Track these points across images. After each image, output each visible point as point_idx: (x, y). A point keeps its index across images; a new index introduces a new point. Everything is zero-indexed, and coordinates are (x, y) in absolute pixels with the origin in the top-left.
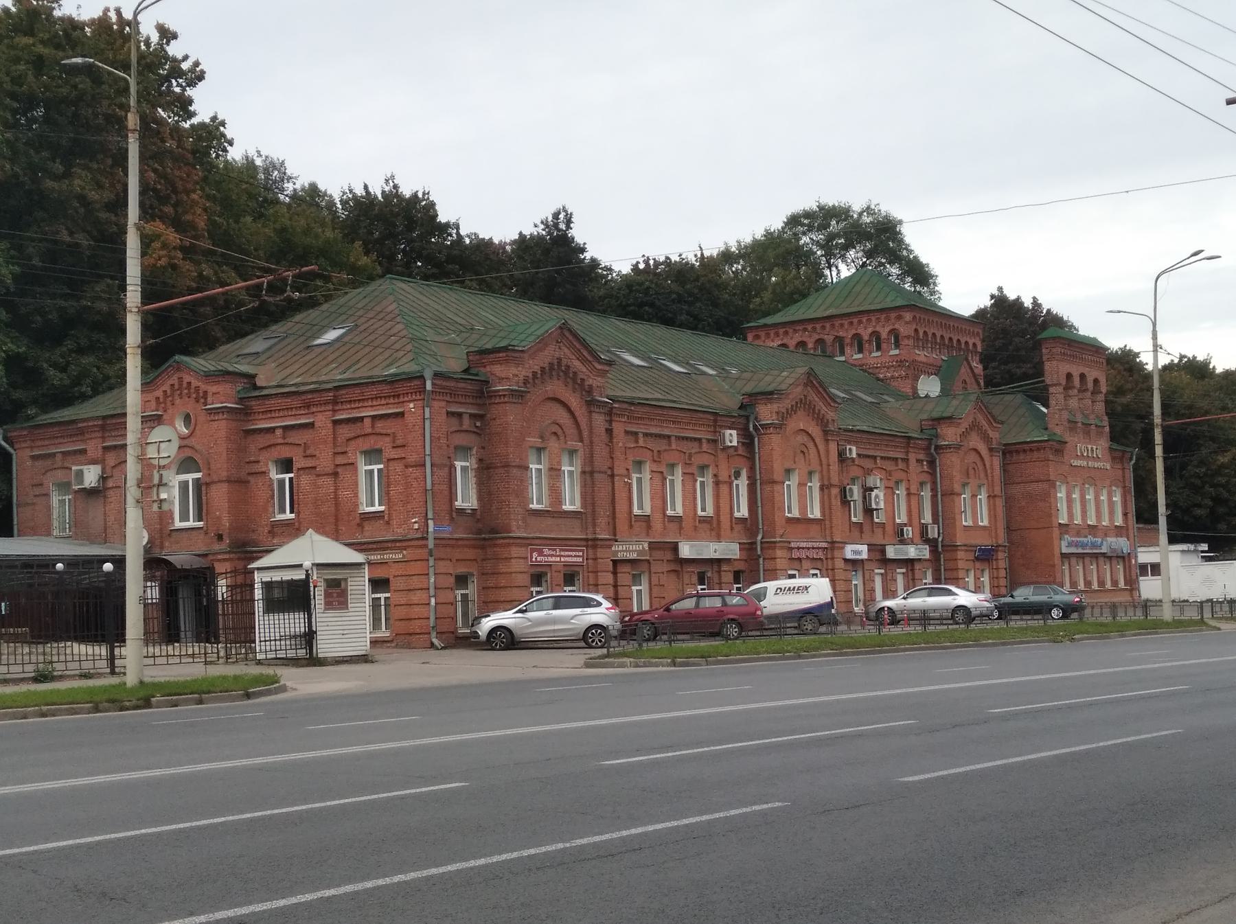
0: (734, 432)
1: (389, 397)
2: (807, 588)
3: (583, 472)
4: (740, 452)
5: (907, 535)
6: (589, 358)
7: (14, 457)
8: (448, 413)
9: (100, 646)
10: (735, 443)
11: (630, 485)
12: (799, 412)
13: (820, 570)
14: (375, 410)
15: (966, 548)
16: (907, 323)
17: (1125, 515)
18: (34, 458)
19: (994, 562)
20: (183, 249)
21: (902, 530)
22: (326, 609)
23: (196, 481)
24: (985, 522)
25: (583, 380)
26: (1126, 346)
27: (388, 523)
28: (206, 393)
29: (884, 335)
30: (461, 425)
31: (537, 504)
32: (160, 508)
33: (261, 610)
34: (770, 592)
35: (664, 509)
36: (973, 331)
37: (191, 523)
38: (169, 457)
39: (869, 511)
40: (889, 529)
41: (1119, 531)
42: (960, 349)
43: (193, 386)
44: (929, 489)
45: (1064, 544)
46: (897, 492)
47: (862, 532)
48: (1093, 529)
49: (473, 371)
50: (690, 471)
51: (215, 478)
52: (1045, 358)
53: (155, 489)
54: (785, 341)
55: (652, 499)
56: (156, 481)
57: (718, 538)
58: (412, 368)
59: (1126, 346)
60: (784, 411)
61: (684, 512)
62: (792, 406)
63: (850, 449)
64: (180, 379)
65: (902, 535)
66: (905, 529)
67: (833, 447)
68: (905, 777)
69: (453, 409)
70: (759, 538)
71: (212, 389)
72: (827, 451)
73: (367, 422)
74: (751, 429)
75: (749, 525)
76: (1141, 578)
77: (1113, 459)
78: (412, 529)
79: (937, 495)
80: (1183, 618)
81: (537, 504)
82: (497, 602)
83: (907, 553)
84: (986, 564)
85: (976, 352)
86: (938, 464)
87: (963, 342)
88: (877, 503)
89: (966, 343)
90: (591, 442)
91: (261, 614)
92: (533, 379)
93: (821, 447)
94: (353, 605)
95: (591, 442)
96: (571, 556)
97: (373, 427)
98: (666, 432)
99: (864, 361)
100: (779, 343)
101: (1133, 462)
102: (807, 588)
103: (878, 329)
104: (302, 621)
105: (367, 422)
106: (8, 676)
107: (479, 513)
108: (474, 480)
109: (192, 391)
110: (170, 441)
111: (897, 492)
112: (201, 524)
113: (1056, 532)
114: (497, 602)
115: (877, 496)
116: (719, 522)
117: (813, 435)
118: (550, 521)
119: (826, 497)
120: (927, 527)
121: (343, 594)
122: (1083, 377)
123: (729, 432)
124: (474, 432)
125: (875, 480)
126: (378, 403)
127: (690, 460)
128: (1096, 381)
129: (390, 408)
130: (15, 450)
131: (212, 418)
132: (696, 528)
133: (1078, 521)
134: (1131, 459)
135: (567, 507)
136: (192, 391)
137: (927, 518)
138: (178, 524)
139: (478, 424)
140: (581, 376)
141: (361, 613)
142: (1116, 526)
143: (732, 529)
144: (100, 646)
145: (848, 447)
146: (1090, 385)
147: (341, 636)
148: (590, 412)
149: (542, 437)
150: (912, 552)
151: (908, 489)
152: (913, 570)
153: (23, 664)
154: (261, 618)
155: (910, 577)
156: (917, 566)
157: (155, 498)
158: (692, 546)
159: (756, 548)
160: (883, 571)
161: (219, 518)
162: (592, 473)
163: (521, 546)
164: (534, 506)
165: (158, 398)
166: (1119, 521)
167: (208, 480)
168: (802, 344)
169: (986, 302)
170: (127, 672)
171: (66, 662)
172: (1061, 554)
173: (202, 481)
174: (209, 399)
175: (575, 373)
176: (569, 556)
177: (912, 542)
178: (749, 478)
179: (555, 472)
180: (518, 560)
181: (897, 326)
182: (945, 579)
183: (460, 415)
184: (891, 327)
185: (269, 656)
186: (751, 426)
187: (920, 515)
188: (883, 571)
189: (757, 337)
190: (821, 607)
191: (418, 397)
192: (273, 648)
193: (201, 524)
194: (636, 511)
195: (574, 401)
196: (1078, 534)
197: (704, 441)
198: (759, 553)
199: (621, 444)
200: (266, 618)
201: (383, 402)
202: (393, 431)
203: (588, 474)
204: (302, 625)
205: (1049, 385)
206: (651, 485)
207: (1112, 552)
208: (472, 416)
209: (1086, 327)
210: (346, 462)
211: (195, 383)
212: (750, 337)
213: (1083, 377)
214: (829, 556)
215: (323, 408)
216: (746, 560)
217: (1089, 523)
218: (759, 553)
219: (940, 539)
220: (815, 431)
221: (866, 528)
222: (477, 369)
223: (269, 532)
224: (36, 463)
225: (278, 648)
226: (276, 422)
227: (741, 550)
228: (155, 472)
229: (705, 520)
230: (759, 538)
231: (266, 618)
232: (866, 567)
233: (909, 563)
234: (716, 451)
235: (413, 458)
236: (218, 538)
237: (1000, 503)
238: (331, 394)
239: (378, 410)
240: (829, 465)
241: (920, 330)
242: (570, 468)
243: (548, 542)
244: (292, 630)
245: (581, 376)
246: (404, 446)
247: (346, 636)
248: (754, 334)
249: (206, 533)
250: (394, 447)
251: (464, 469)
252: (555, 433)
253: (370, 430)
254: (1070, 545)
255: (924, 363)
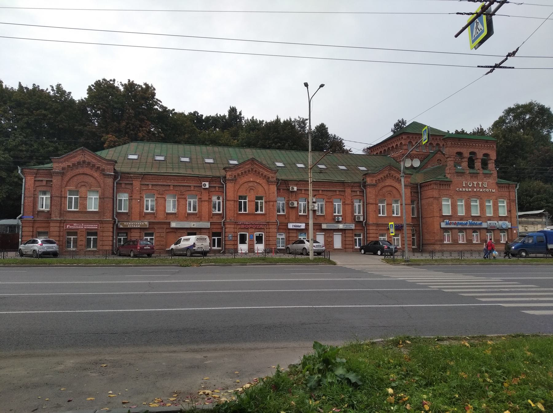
8: (351, 191)
15: (376, 225)
16: (405, 139)
26: (253, 117)
31: (74, 209)
59: (253, 117)
68: (524, 310)
80: (443, 257)
81: (74, 209)
84: (400, 232)
96: (91, 226)
98: (169, 184)
99: (394, 156)
118: (80, 214)
160: (324, 233)
168: (377, 153)
169: (224, 112)
172: (441, 228)
176: (88, 226)
186: (222, 181)
188: (324, 233)
209: (206, 112)
243: (76, 222)
254: (447, 224)
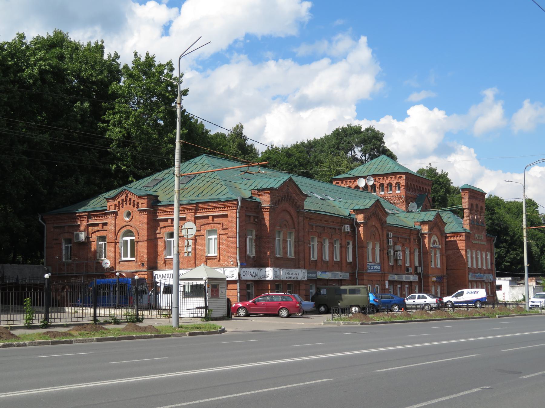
0: (348, 226)
1: (221, 208)
2: (477, 292)
3: (295, 242)
4: (350, 234)
5: (410, 271)
6: (299, 193)
7: (45, 227)
8: (245, 215)
10: (349, 230)
11: (310, 247)
12: (373, 218)
13: (379, 285)
14: (214, 213)
17: (491, 264)
18: (55, 228)
19: (442, 284)
20: (491, 214)
21: (408, 269)
22: (211, 297)
23: (132, 241)
24: (439, 266)
25: (296, 202)
27: (219, 261)
28: (138, 203)
29: (394, 184)
30: (250, 220)
32: (188, 255)
33: (181, 296)
34: (465, 293)
35: (405, 264)
36: (428, 184)
37: (129, 258)
38: (192, 235)
39: (396, 261)
40: (403, 268)
41: (489, 272)
42: (423, 191)
43: (132, 200)
44: (339, 244)
45: (470, 276)
46: (335, 245)
47: (393, 269)
48: (480, 271)
49: (253, 198)
50: (332, 242)
51: (141, 239)
53: (186, 248)
55: (318, 253)
56: (186, 244)
57: (341, 271)
58: (233, 197)
60: (368, 217)
61: (329, 259)
62: (371, 215)
63: (390, 234)
64: (127, 196)
65: (408, 271)
66: (409, 268)
67: (385, 232)
69: (248, 214)
70: (357, 271)
71: (141, 201)
72: (383, 234)
73: (211, 218)
74: (354, 225)
75: (353, 266)
76: (497, 291)
77: (487, 240)
78: (230, 264)
79: (421, 254)
83: (410, 279)
85: (417, 189)
86: (421, 241)
87: (415, 185)
88: (400, 257)
89: (426, 189)
90: (298, 229)
91: (182, 298)
92: (278, 202)
93: (380, 233)
94: (221, 296)
95: (298, 229)
97: (213, 220)
99: (385, 195)
100: (348, 186)
101: (495, 242)
102: (477, 292)
103: (391, 182)
104: (202, 301)
105: (211, 218)
106: (72, 323)
107: (255, 257)
108: (254, 244)
109: (132, 202)
110: (192, 228)
111: (335, 245)
112: (133, 259)
113: (467, 271)
115: (399, 254)
116: (342, 264)
117: (378, 227)
119: (382, 254)
120: (417, 268)
121: (218, 291)
122: (477, 205)
123: (346, 226)
124: (254, 224)
125: (399, 247)
126: (215, 210)
127: (331, 237)
129: (221, 212)
130: (46, 224)
132: (333, 266)
133: (475, 266)
134: (494, 241)
135: (289, 256)
136: (132, 202)
137: (417, 264)
138: (123, 259)
139: (256, 220)
140: (296, 201)
141: (223, 299)
142: (488, 269)
143: (346, 266)
145: (389, 233)
146: (479, 208)
147: (216, 309)
148: (298, 216)
149: (280, 226)
150: (412, 278)
151: (341, 244)
152: (411, 286)
153: (14, 320)
154: (182, 300)
155: (410, 289)
156: (413, 284)
157: (186, 251)
158: (333, 274)
159: (355, 275)
161: (143, 256)
162: (298, 242)
164: (277, 255)
165: (115, 205)
167: (138, 240)
171: (147, 315)
172: (469, 280)
173: (135, 241)
174: (140, 206)
175: (293, 200)
177: (411, 274)
178: (353, 245)
179: (285, 241)
181: (399, 181)
182: (424, 290)
183: (250, 216)
184: (397, 181)
185: (186, 316)
187: (414, 263)
189: (338, 183)
190: (482, 299)
191: (234, 208)
192: (188, 313)
193: (133, 259)
194: (312, 258)
195: (292, 211)
196: (475, 273)
197: (337, 229)
198: (357, 277)
199: (307, 230)
200: (184, 300)
201: (218, 210)
202: (222, 222)
203: (297, 241)
204: (202, 303)
206: (317, 247)
207: (487, 280)
208: (254, 217)
210: (200, 234)
211: (133, 199)
213: (477, 205)
214: (383, 279)
215: (190, 211)
216: (351, 280)
218: (357, 277)
219: (422, 273)
220: (378, 226)
221: (395, 268)
222: (255, 197)
223: (164, 263)
224: (56, 230)
225: (190, 313)
226: (168, 216)
227: (350, 276)
228: (186, 240)
229: (337, 263)
230: (357, 271)
231: (184, 300)
232: (394, 285)
233: (410, 283)
234: (341, 234)
235: (231, 234)
236: (142, 265)
237: (444, 258)
238: (194, 206)
239: (215, 213)
240: (383, 241)
241: (408, 183)
242: (290, 240)
244: (196, 305)
245: (296, 201)
246: (227, 229)
247: (219, 309)
249: (137, 262)
250: (222, 229)
251: (250, 239)
252: (285, 225)
253: (212, 222)
255: (410, 197)
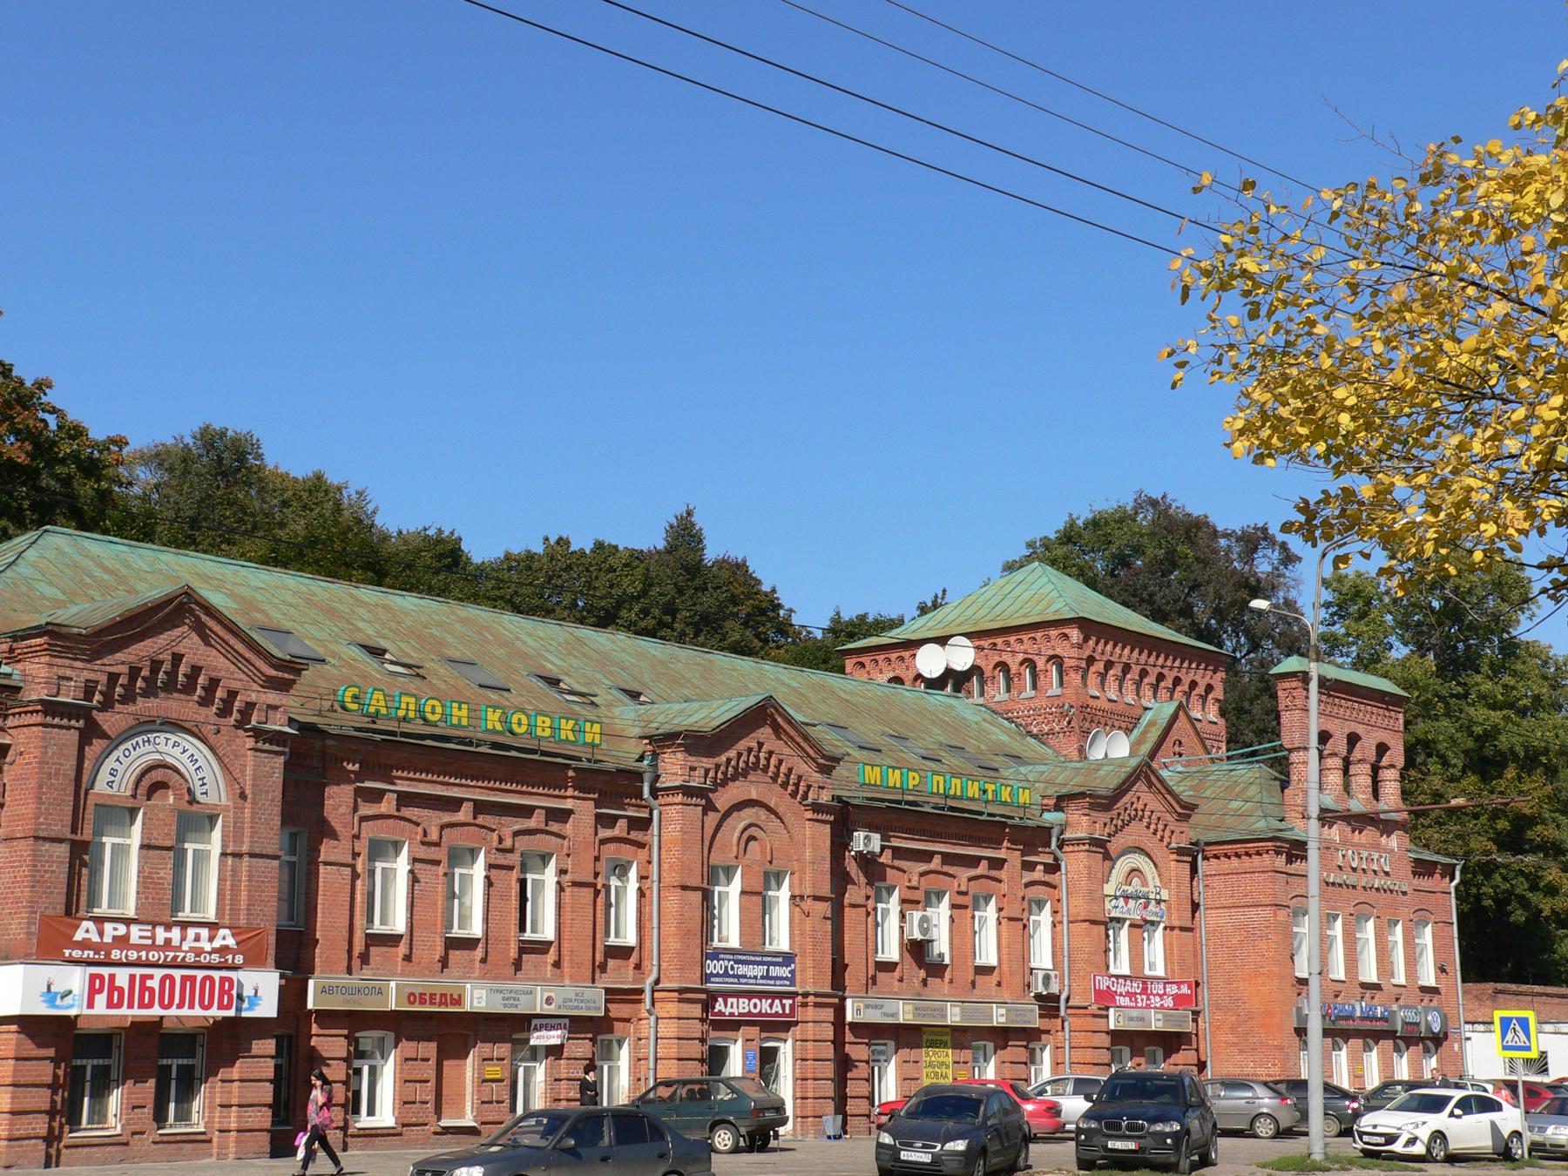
9: (54, 1087)
17: (1442, 970)
52: (1281, 707)
54: (898, 672)
59: (1550, 647)
82: (679, 1019)
100: (891, 675)
114: (679, 1019)
128: (1382, 749)
131: (260, 745)
133: (1401, 979)
144: (54, 1087)
163: (69, 885)
166: (1429, 977)
170: (53, 1170)
180: (823, 1076)
205: (272, 1057)
212: (849, 664)
217: (1297, 974)
248: (854, 661)
